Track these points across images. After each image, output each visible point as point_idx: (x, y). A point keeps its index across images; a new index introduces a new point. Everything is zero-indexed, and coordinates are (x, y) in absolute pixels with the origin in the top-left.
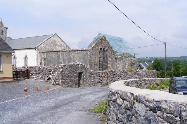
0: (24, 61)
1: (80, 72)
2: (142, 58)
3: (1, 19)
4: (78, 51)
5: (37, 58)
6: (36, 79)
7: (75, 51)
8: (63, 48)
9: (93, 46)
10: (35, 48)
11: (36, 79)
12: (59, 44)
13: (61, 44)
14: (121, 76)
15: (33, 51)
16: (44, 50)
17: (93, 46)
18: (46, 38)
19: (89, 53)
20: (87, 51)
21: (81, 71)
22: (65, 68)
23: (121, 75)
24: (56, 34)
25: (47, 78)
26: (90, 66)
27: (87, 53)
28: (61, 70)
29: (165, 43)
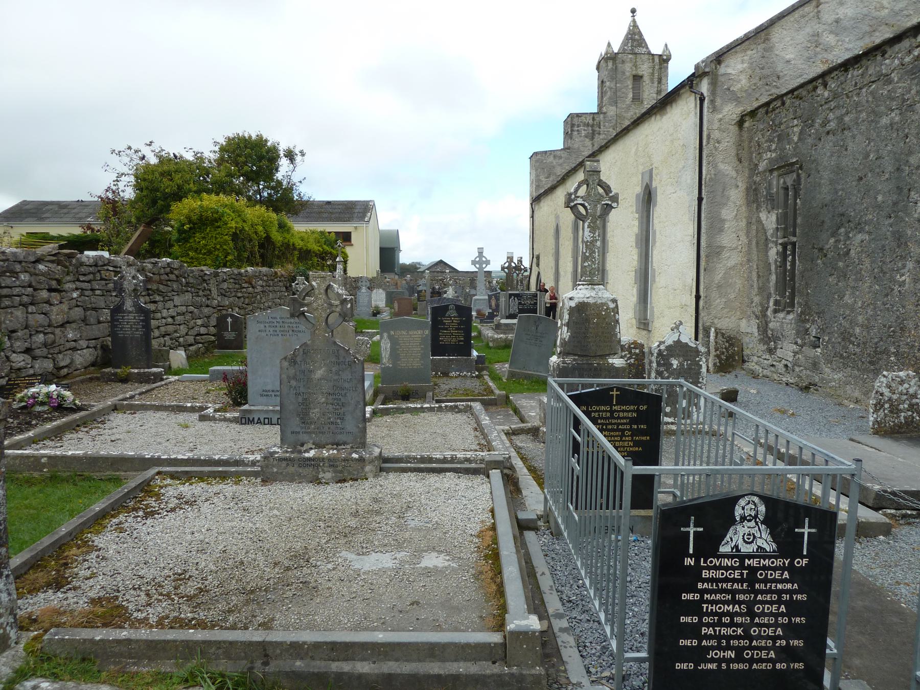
3: (633, 11)
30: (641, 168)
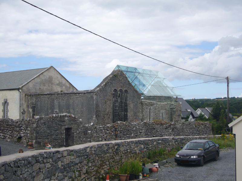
0: (2, 109)
1: (66, 127)
2: (217, 98)
4: (80, 93)
5: (22, 104)
6: (3, 137)
7: (75, 93)
8: (64, 87)
9: (102, 87)
10: (18, 89)
11: (3, 137)
12: (58, 82)
13: (62, 82)
14: (141, 133)
15: (16, 94)
16: (33, 91)
17: (102, 87)
18: (37, 74)
19: (95, 97)
20: (92, 94)
21: (70, 126)
22: (42, 121)
23: (142, 130)
24: (52, 67)
25: (17, 137)
26: (96, 116)
27: (92, 97)
28: (35, 125)
29: (228, 78)
30: (4, 98)
